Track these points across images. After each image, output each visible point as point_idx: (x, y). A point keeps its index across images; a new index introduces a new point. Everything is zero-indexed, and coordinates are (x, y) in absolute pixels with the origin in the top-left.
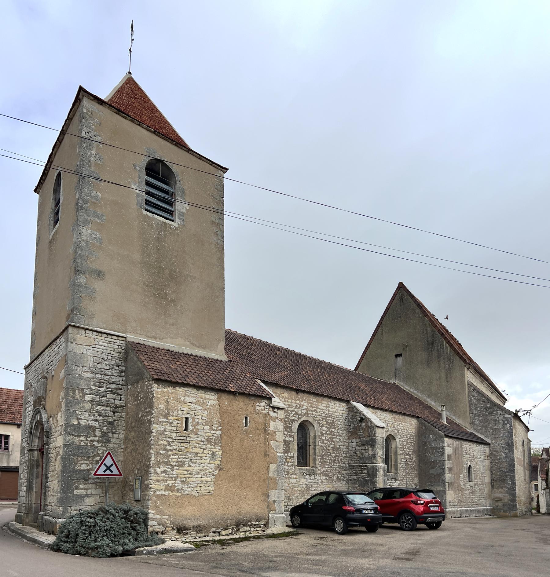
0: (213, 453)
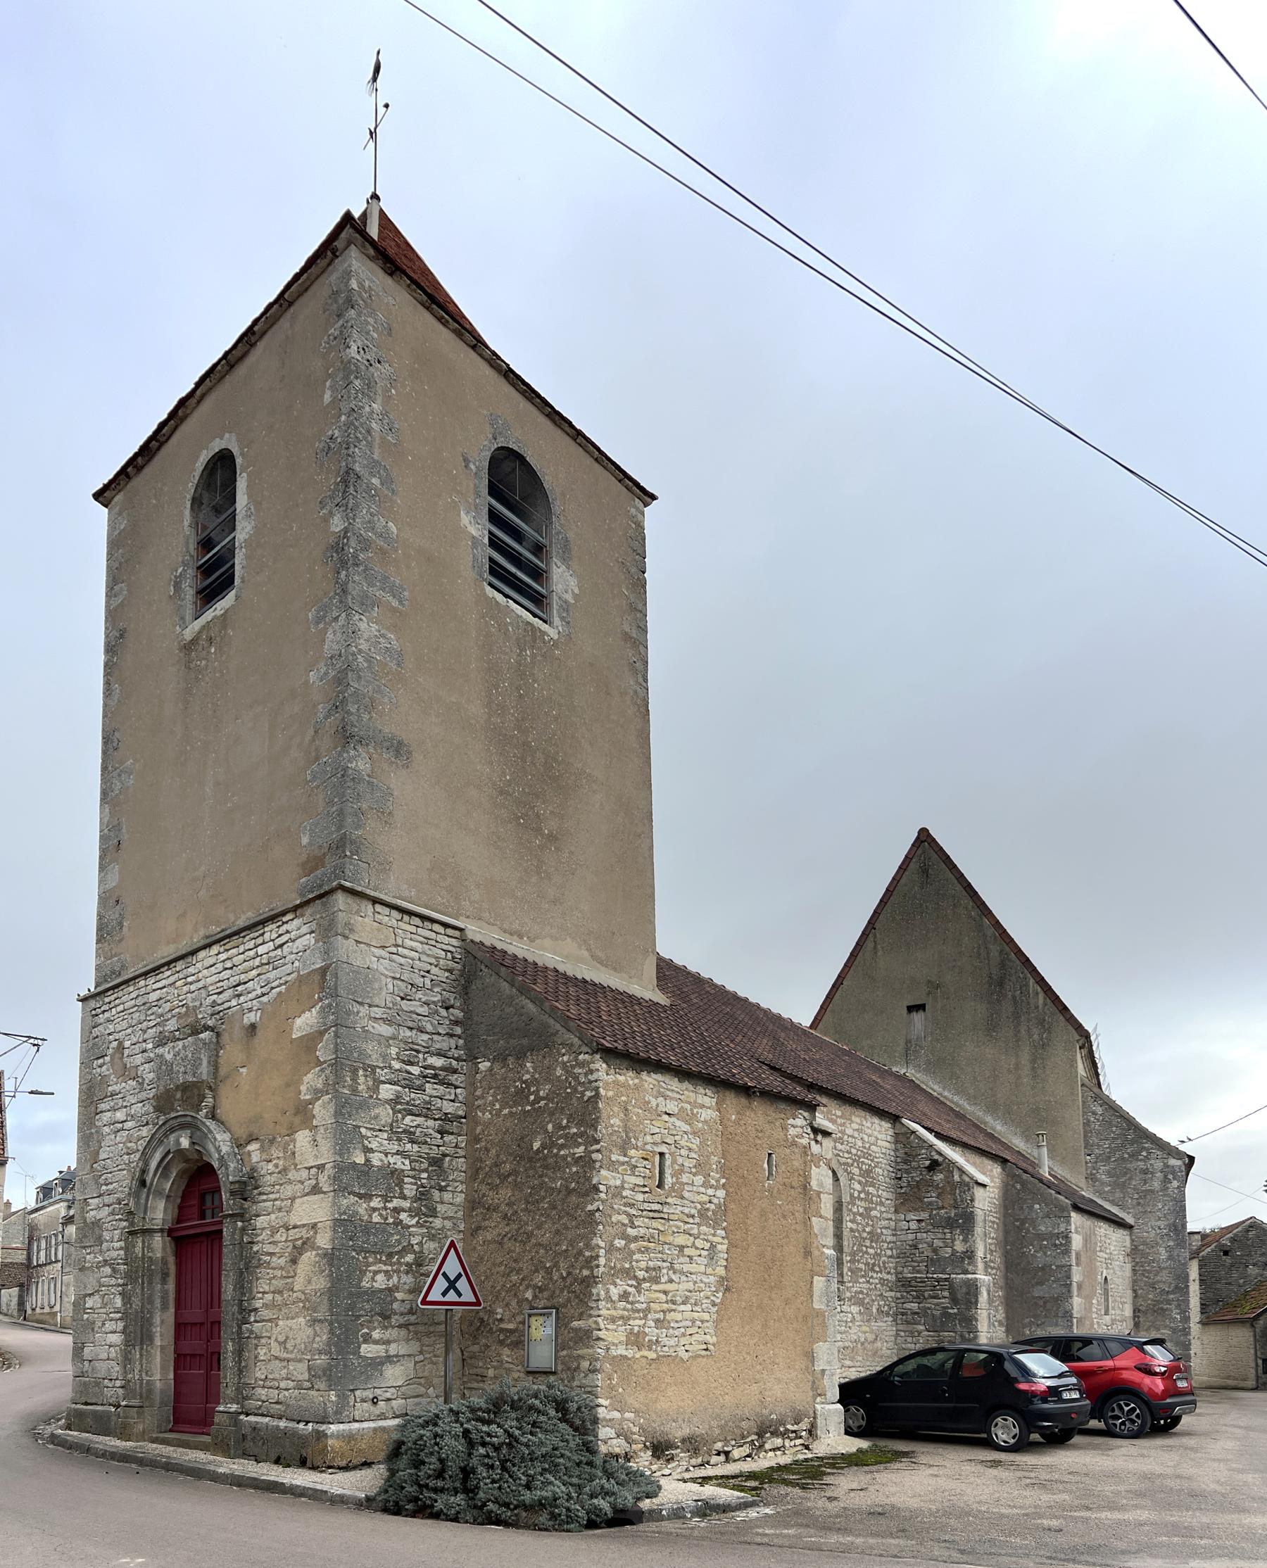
0: (713, 1247)
